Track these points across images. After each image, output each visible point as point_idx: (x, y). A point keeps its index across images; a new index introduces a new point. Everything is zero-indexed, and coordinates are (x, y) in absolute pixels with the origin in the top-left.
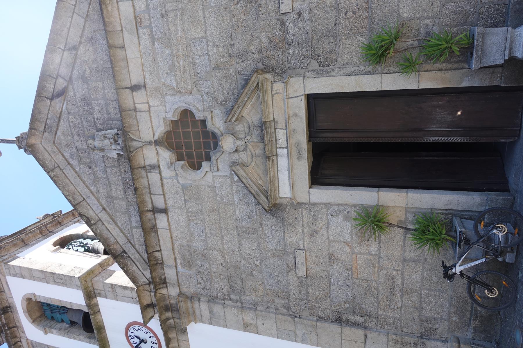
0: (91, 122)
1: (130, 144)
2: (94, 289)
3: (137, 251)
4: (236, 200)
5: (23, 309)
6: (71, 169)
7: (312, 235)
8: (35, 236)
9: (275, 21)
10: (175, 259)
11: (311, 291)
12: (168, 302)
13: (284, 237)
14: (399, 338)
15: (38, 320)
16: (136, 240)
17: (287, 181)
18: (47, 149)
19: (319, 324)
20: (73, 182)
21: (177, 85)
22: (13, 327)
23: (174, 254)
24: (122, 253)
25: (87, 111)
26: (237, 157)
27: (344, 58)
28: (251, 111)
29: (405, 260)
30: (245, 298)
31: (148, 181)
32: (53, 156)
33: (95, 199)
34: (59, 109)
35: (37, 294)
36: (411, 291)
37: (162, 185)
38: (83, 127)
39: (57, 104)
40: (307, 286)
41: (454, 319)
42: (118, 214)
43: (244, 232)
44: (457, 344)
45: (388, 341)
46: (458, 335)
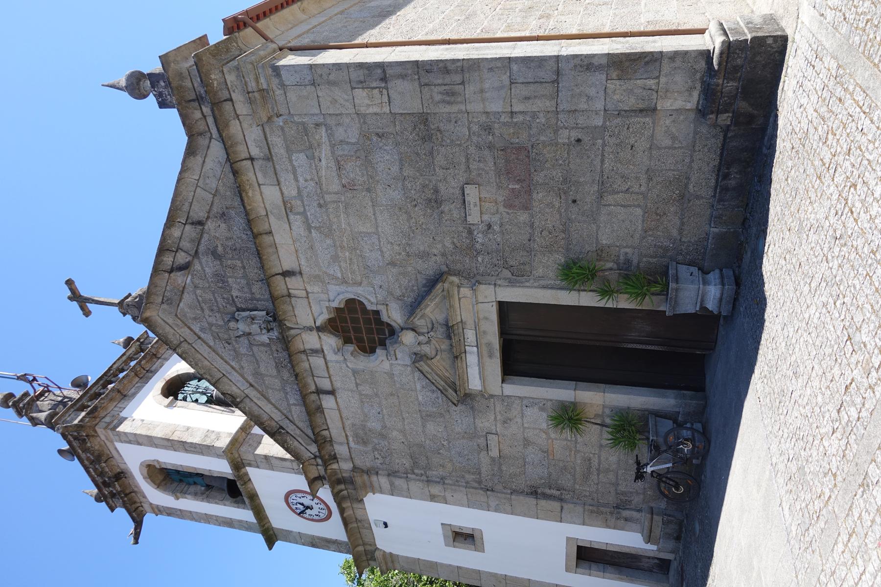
0: (228, 299)
1: (287, 334)
2: (241, 460)
3: (297, 427)
4: (419, 387)
5: (142, 474)
6: (203, 344)
7: (505, 422)
8: (130, 382)
9: (461, 229)
10: (346, 436)
11: (504, 468)
12: (340, 476)
13: (475, 423)
14: (595, 509)
15: (162, 484)
16: (295, 416)
17: (478, 376)
18: (168, 321)
19: (513, 497)
20: (207, 358)
21: (342, 276)
22: (131, 493)
23: (345, 432)
24: (278, 429)
25: (221, 288)
26: (419, 349)
27: (540, 271)
28: (434, 310)
29: (601, 446)
30: (429, 473)
31: (310, 364)
32: (176, 329)
33: (238, 375)
34: (182, 282)
35: (160, 460)
36: (607, 471)
37: (327, 367)
38: (217, 303)
39: (179, 278)
40: (501, 465)
41: (649, 493)
42: (270, 391)
43: (427, 415)
44: (650, 516)
45: (584, 511)
46: (653, 505)
